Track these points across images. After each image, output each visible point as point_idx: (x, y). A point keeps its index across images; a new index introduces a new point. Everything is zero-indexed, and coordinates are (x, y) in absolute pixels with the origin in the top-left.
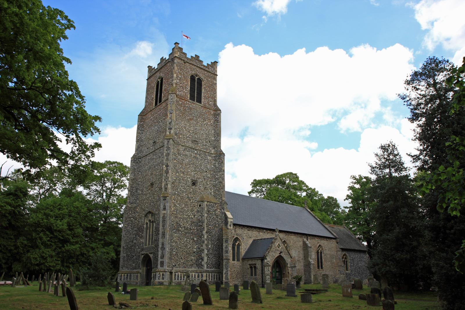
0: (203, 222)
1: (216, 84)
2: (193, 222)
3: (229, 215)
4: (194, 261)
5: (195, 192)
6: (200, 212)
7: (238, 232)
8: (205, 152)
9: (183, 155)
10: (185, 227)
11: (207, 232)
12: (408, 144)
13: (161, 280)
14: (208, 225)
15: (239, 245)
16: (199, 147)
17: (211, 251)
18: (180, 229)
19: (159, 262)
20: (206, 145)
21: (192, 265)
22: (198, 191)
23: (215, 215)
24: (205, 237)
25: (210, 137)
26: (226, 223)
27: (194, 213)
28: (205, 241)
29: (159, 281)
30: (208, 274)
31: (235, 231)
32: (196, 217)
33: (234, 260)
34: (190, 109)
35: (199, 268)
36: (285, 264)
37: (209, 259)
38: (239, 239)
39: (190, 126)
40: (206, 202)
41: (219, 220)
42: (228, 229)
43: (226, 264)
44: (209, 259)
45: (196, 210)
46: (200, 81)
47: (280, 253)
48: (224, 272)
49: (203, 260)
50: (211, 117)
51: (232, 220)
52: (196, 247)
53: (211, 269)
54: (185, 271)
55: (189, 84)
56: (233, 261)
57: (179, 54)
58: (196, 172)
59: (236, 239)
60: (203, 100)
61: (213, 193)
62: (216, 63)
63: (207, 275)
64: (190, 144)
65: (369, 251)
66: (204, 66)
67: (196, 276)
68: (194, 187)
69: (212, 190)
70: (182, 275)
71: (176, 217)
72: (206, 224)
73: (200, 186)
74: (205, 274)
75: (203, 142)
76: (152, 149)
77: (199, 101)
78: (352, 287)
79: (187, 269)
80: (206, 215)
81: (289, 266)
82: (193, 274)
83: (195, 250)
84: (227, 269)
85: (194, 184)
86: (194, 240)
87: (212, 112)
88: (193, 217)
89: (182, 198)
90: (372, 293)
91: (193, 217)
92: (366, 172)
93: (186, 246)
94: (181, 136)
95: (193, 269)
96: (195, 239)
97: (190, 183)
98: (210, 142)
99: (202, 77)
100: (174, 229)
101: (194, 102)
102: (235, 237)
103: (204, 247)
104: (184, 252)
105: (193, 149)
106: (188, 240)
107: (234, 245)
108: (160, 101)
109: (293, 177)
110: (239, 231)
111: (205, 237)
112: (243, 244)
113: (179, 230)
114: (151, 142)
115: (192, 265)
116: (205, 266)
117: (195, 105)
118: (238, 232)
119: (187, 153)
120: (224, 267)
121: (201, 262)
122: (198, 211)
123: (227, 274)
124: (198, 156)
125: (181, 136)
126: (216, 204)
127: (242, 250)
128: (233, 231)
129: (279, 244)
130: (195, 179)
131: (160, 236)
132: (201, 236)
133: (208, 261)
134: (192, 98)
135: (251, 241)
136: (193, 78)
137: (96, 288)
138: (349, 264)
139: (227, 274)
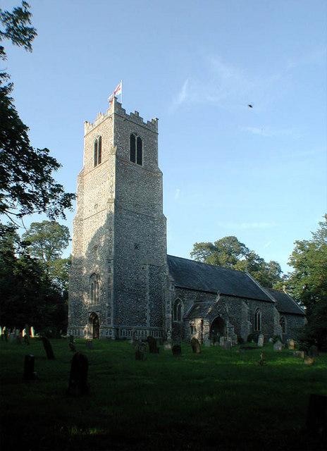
1: (157, 143)
14: (151, 287)
34: (131, 171)
65: (309, 313)
66: (144, 124)
74: (148, 332)
76: (94, 211)
77: (140, 163)
78: (155, 352)
85: (136, 247)
92: (309, 238)
97: (133, 247)
108: (100, 162)
109: (233, 240)
114: (93, 205)
117: (135, 166)
119: (130, 217)
134: (133, 159)
136: (132, 138)
137: (308, 368)
138: (286, 327)
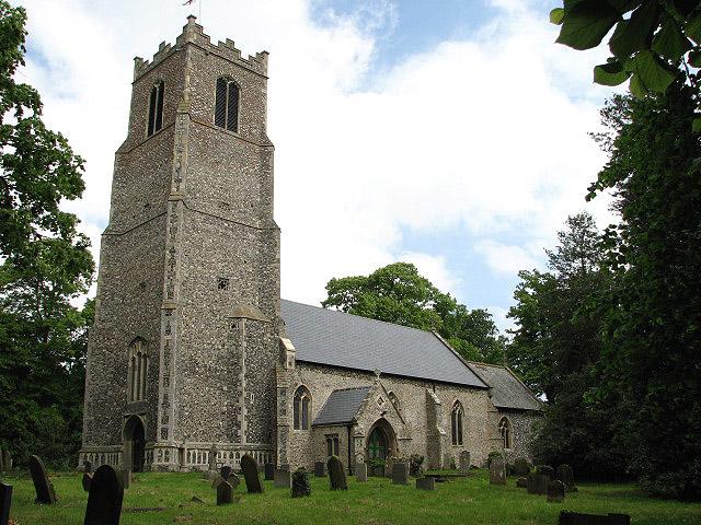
2: (220, 358)
3: (288, 344)
5: (223, 301)
16: (233, 215)
17: (254, 411)
19: (159, 430)
26: (283, 359)
31: (300, 374)
33: (296, 427)
36: (392, 435)
46: (235, 88)
51: (293, 354)
59: (302, 389)
73: (234, 289)
80: (245, 344)
81: (398, 437)
87: (258, 150)
89: (201, 312)
93: (208, 401)
96: (225, 388)
99: (239, 80)
103: (242, 401)
107: (297, 399)
110: (307, 374)
113: (195, 372)
116: (244, 437)
122: (230, 337)
128: (296, 374)
131: (161, 382)
132: (235, 383)
134: (220, 121)
135: (328, 393)
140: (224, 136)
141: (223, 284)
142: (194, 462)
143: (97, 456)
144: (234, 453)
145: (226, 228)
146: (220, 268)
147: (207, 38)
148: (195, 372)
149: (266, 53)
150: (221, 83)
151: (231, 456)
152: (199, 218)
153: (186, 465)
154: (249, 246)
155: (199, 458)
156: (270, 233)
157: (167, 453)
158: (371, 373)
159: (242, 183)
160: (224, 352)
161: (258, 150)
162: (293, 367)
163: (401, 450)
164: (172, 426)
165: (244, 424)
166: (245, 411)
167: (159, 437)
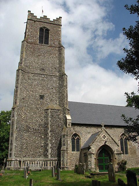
0: (48, 124)
2: (40, 125)
3: (69, 117)
4: (42, 153)
5: (42, 104)
6: (46, 117)
7: (77, 129)
8: (51, 75)
9: (32, 79)
10: (34, 129)
11: (51, 131)
12: (110, 40)
13: (9, 167)
15: (78, 140)
16: (47, 72)
17: (54, 145)
18: (30, 130)
19: (9, 154)
20: (52, 71)
21: (40, 155)
22: (45, 102)
23: (59, 118)
24: (50, 135)
25: (55, 65)
26: (66, 123)
27: (42, 118)
28: (49, 137)
29: (8, 167)
30: (51, 162)
31: (74, 129)
32: (43, 121)
33: (73, 150)
35: (45, 158)
36: (112, 152)
37: (53, 150)
38: (78, 135)
39: (38, 60)
40: (50, 110)
41: (62, 122)
42: (67, 127)
43: (63, 154)
44: (53, 150)
45: (43, 116)
46: (47, 30)
47: (105, 143)
48: (61, 160)
49: (48, 152)
50: (56, 52)
51: (71, 121)
52: (43, 142)
53: (55, 158)
54: (33, 160)
55: (39, 34)
56: (72, 151)
57: (30, 17)
58: (43, 90)
59: (76, 135)
60: (49, 42)
61: (58, 103)
62: (60, 18)
63: (45, 163)
64: (38, 72)
66: (51, 21)
67: (43, 163)
68: (41, 100)
69: (58, 101)
70: (31, 163)
71: (26, 122)
72: (50, 126)
73: (47, 99)
75: (50, 69)
79: (35, 158)
80: (50, 119)
81: (115, 152)
82: (41, 162)
83: (43, 145)
84: (63, 157)
86: (41, 137)
87: (57, 49)
88: (40, 121)
89: (31, 109)
90: (103, 168)
91: (40, 121)
93: (35, 142)
94: (31, 67)
95: (41, 158)
96: (43, 137)
98: (55, 68)
99: (48, 27)
100: (24, 131)
101: (42, 44)
102: (73, 134)
103: (49, 142)
104: (33, 146)
105: (41, 74)
106: (36, 137)
107: (73, 139)
110: (78, 129)
111: (50, 135)
112: (81, 138)
113: (29, 131)
115: (40, 155)
116: (50, 156)
118: (77, 129)
120: (61, 156)
121: (47, 153)
122: (45, 117)
123: (64, 161)
124: (45, 79)
125: (31, 67)
126: (59, 110)
127: (81, 143)
128: (72, 129)
129: (104, 136)
130: (43, 95)
131: (10, 135)
132: (46, 134)
133: (51, 152)
134: (41, 42)
135: (89, 136)
139: (63, 161)
140: (45, 48)
141: (42, 97)
142: (45, 166)
143: (45, 163)
144: (34, 162)
145: (43, 77)
146: (40, 91)
147: (36, 17)
148: (29, 131)
149: (61, 17)
150: (41, 29)
151: (37, 164)
152: (31, 76)
153: (22, 167)
154: (55, 82)
155: (45, 164)
156: (62, 77)
157: (10, 163)
158: (99, 126)
159: (51, 61)
160: (42, 123)
161: (57, 49)
162: (70, 126)
163: (117, 158)
164: (13, 152)
165: (50, 151)
166: (50, 145)
167: (9, 156)
